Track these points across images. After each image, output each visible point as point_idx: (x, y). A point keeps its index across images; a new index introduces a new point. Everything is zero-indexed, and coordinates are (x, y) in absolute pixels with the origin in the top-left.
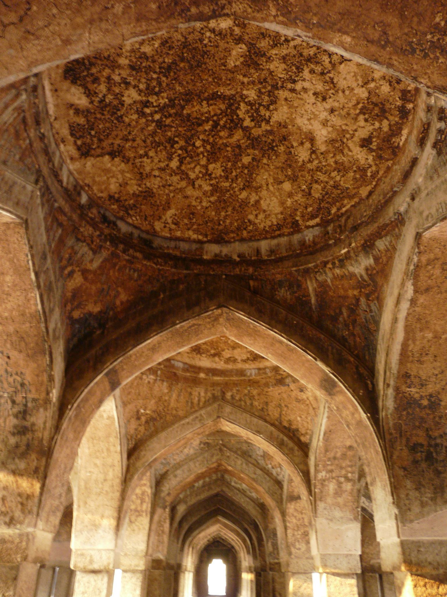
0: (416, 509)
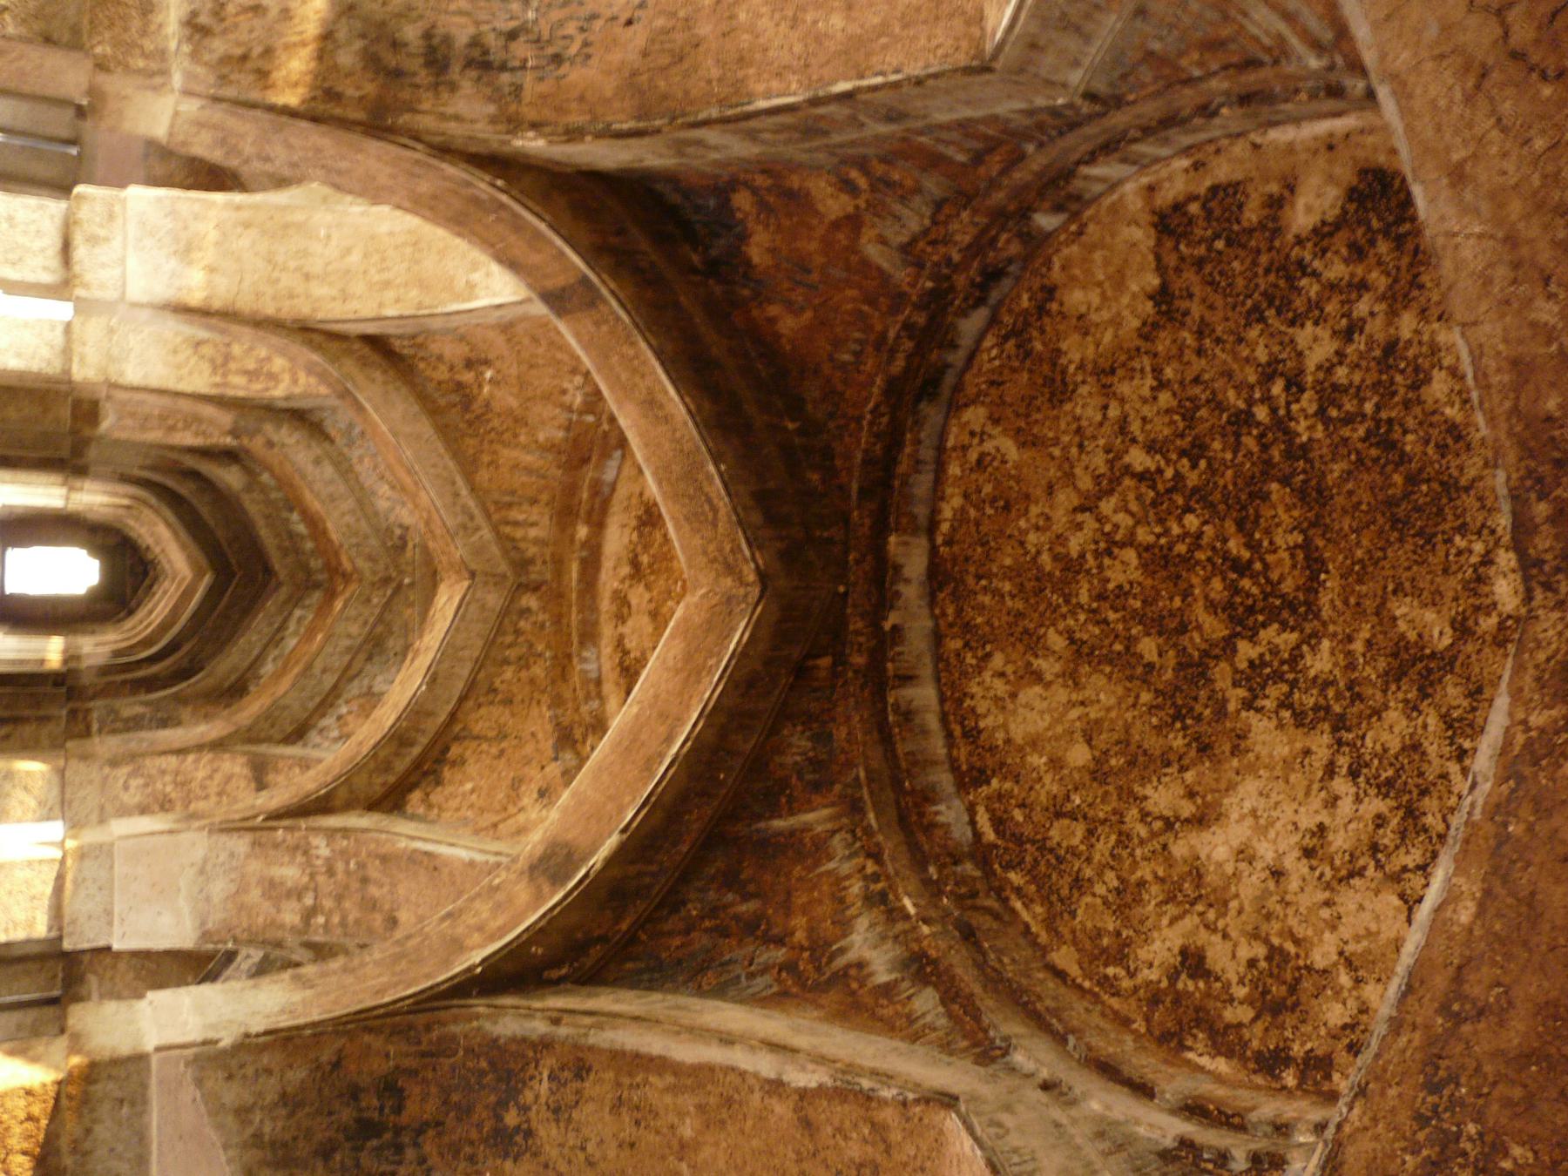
0: (232, 1094)
